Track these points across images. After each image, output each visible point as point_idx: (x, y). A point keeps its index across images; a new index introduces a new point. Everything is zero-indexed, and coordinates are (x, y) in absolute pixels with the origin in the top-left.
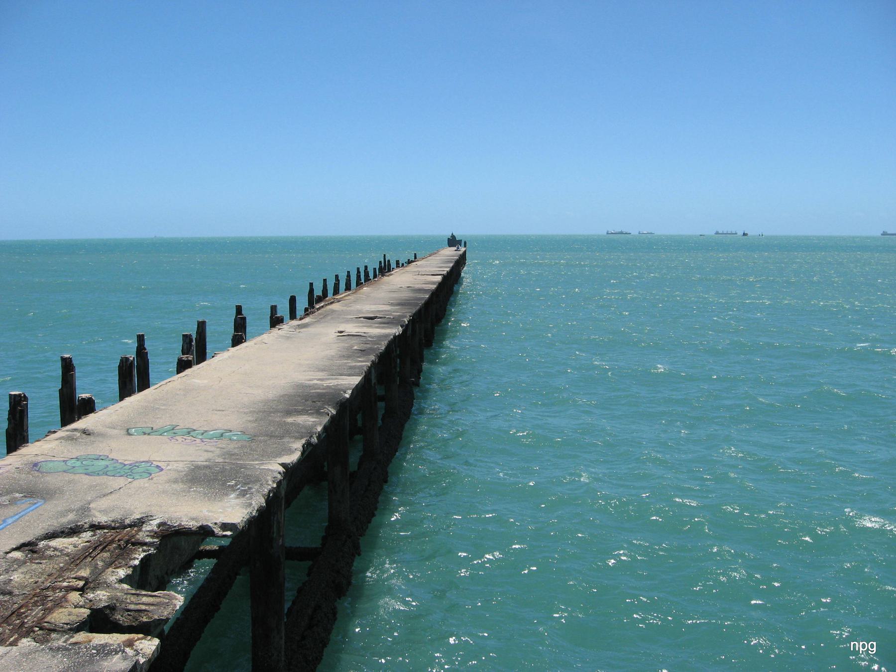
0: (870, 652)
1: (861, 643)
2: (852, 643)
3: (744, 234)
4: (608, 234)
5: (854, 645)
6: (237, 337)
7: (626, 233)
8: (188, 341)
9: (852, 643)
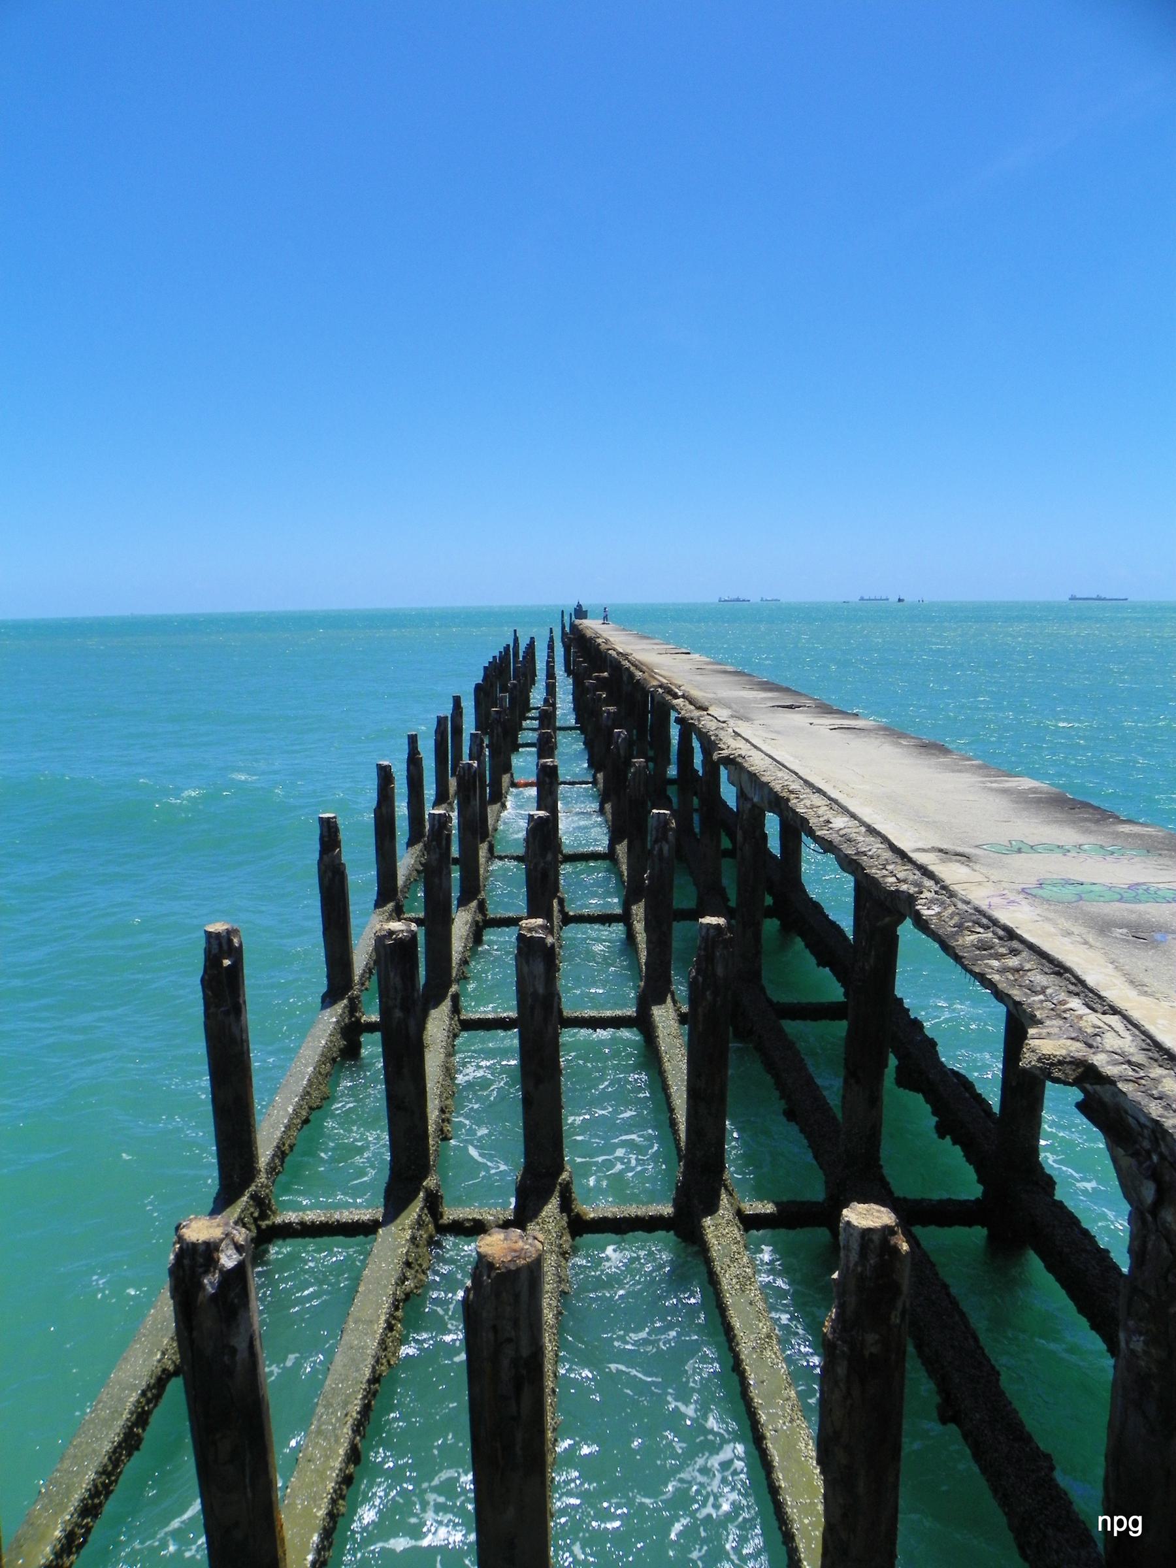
0: (1131, 1533)
1: (1116, 1519)
2: (1115, 1517)
3: (900, 600)
4: (720, 601)
5: (1105, 1521)
6: (546, 736)
7: (744, 601)
8: (478, 742)
9: (1115, 1517)
